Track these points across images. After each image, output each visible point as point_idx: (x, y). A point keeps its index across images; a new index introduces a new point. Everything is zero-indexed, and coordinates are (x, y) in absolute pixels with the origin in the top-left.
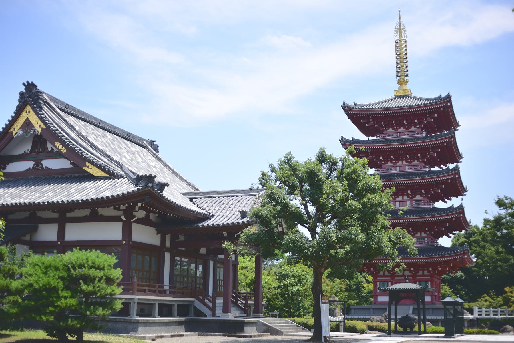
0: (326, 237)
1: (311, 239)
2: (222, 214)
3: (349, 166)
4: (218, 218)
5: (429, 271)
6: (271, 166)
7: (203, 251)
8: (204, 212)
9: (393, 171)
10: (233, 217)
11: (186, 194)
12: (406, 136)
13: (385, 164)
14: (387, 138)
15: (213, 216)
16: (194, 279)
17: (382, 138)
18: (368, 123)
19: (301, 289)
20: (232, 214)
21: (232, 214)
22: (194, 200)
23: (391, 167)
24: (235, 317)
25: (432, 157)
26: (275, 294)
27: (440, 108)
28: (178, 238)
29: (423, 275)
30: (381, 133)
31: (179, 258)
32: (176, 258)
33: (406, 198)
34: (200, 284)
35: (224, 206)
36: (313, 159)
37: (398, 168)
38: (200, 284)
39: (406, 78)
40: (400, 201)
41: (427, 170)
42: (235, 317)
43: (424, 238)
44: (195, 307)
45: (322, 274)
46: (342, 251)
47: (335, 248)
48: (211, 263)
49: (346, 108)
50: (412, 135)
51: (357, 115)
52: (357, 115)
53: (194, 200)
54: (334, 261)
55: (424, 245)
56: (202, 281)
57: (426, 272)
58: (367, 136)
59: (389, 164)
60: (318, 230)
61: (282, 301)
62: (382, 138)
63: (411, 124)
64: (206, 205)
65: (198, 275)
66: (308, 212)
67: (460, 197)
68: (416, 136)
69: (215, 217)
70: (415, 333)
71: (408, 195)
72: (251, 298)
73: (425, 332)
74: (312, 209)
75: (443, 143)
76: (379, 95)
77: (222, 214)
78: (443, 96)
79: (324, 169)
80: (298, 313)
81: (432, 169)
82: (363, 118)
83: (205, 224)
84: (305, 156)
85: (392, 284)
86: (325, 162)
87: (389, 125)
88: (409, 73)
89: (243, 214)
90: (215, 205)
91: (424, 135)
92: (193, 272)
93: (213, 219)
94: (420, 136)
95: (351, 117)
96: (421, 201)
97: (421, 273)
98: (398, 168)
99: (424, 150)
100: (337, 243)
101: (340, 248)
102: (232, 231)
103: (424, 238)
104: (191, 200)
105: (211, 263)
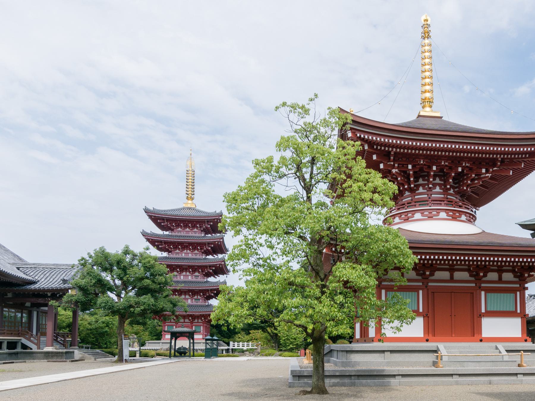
0: (128, 300)
1: (117, 301)
2: (46, 280)
3: (146, 258)
4: (43, 283)
5: (202, 320)
6: (89, 254)
7: (28, 304)
8: (31, 278)
9: (180, 256)
10: (56, 283)
11: (13, 264)
12: (190, 234)
13: (174, 251)
14: (177, 234)
15: (38, 281)
16: (20, 324)
17: (173, 234)
18: (164, 223)
19: (108, 330)
20: (55, 281)
21: (55, 281)
22: (21, 269)
23: (178, 253)
24: (409, 280)
25: (207, 250)
26: (88, 334)
27: (214, 219)
28: (7, 295)
29: (198, 322)
30: (172, 230)
31: (7, 309)
32: (4, 309)
33: (188, 273)
34: (25, 327)
35: (47, 275)
36: (120, 252)
37: (183, 254)
38: (25, 327)
39: (193, 196)
40: (184, 276)
41: (204, 257)
42: (409, 280)
43: (199, 299)
44: (22, 344)
45: (124, 322)
46: (138, 309)
47: (133, 307)
48: (35, 314)
49: (147, 211)
50: (195, 235)
51: (158, 219)
52: (158, 219)
53: (21, 269)
54: (132, 314)
55: (199, 303)
56: (27, 325)
57: (200, 321)
58: (163, 228)
59: (177, 251)
60: (123, 296)
61: (93, 338)
62: (173, 234)
63: (194, 227)
64: (32, 274)
65: (23, 321)
66: (115, 284)
67: (225, 275)
68: (197, 235)
69: (40, 282)
70: (187, 356)
71: (190, 272)
72: (68, 336)
73: (193, 356)
74: (118, 282)
75: (215, 242)
76: (173, 202)
77: (46, 280)
78: (217, 212)
79: (128, 258)
80: (502, 156)
81: (208, 257)
82: (160, 219)
83: (32, 287)
84: (114, 249)
85: (176, 327)
86: (129, 254)
87: (178, 226)
88: (195, 193)
89: (65, 281)
90: (40, 274)
91: (203, 235)
92: (19, 319)
93: (39, 283)
94: (200, 235)
95: (150, 217)
96: (198, 276)
97: (196, 321)
98: (183, 254)
99: (202, 245)
100: (136, 304)
101: (137, 307)
102: (57, 294)
103: (199, 299)
104: (18, 268)
105: (35, 314)
